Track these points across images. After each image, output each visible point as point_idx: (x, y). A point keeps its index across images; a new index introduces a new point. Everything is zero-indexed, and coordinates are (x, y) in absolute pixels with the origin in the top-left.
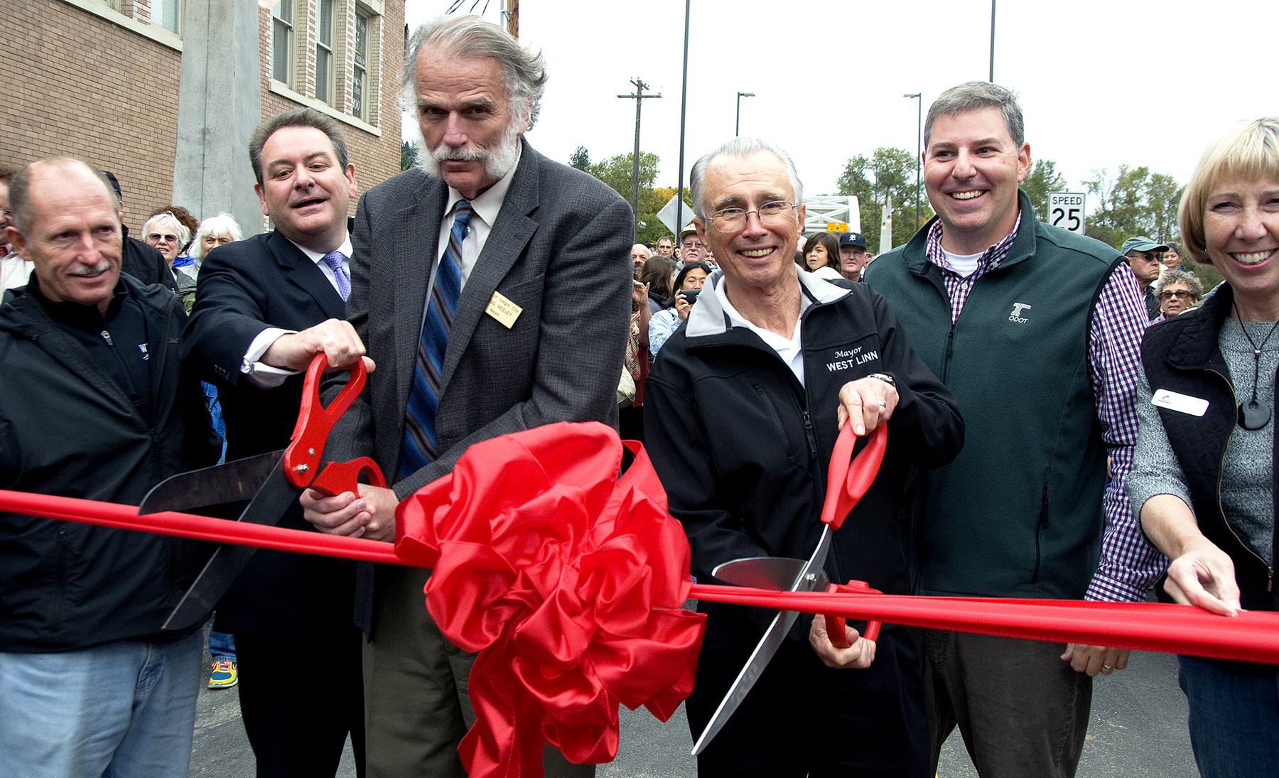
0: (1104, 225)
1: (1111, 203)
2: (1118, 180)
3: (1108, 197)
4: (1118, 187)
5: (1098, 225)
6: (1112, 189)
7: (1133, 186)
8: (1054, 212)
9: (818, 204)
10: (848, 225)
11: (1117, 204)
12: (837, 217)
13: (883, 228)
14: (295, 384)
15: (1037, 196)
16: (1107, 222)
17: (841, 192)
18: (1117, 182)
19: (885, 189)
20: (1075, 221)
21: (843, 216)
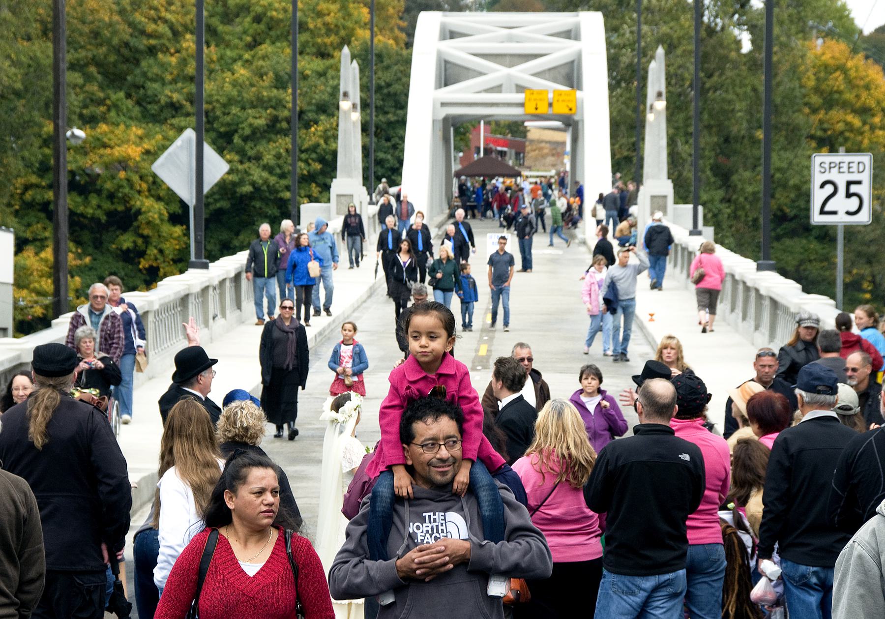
8: (822, 186)
10: (579, 94)
13: (650, 117)
14: (770, 387)
20: (855, 201)
21: (564, 71)
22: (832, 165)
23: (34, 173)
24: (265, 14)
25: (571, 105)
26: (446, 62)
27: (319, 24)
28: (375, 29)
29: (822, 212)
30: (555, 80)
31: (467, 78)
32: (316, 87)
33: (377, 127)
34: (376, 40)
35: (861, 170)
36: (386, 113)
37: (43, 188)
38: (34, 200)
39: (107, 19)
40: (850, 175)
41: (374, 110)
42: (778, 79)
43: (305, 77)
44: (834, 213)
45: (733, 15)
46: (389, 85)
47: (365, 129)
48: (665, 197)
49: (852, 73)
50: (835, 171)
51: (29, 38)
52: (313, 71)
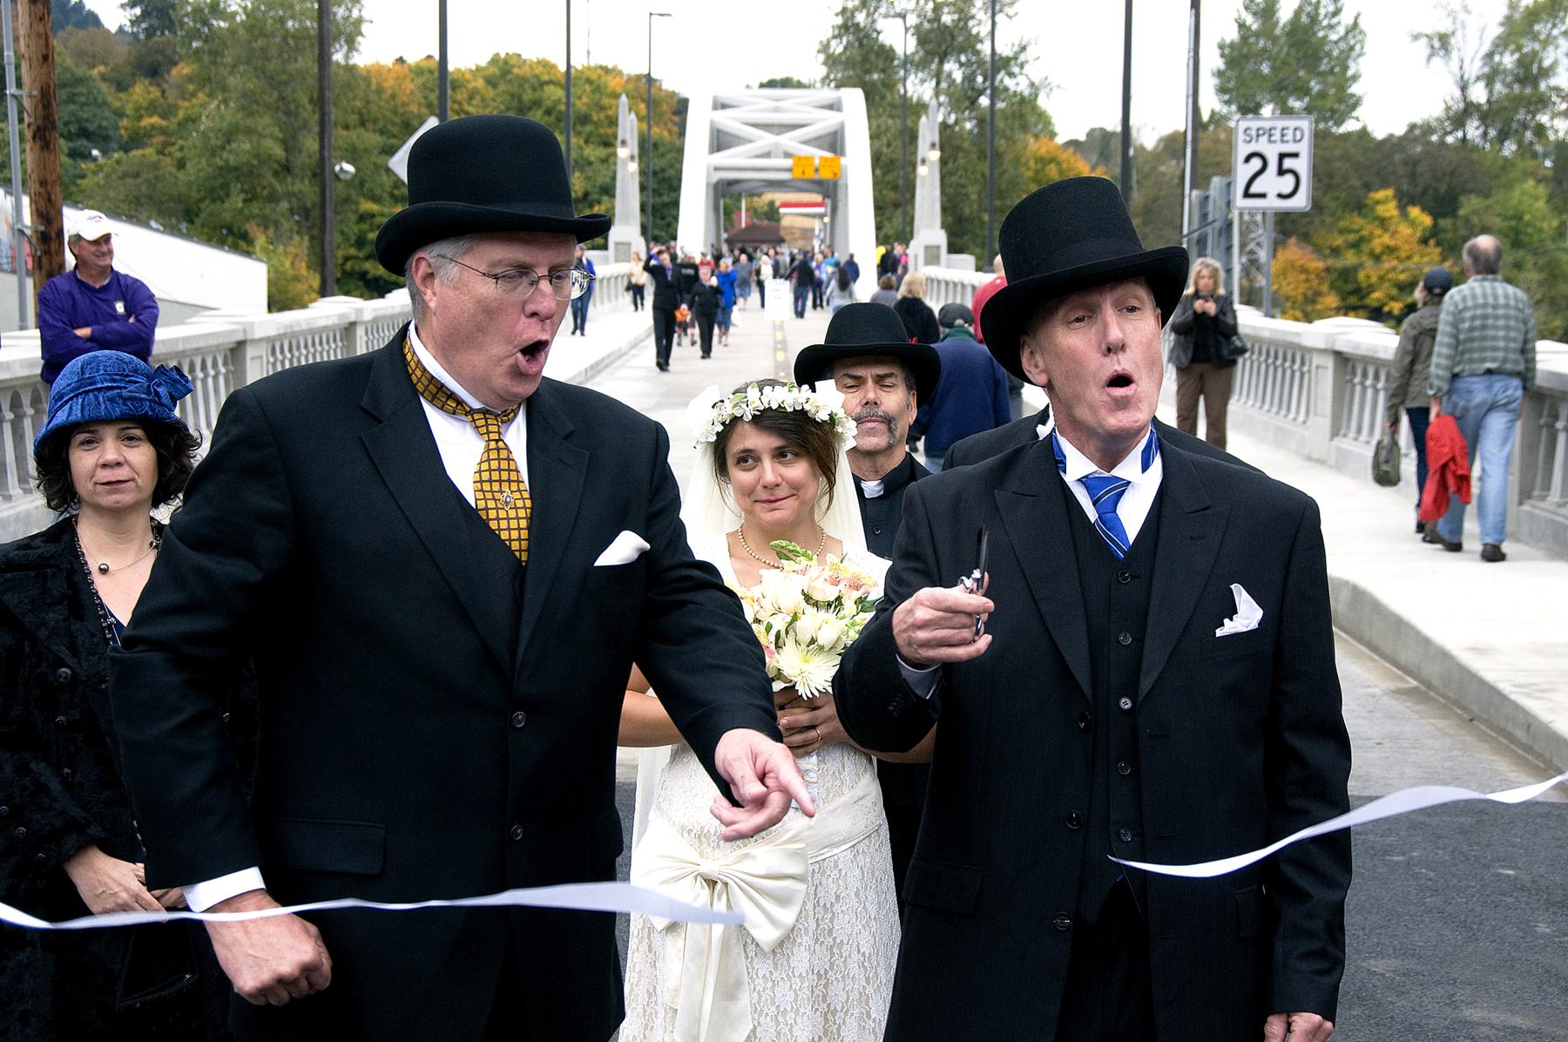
0: (1464, 139)
1: (1481, 85)
2: (1502, 24)
3: (1475, 68)
4: (1501, 44)
5: (1450, 139)
6: (1486, 48)
7: (1535, 37)
8: (1247, 160)
9: (765, 110)
11: (1498, 87)
12: (815, 141)
13: (922, 171)
15: (1302, 73)
16: (1473, 130)
17: (827, 77)
18: (1499, 31)
19: (934, 66)
20: (1289, 179)
22: (1261, 132)
23: (352, 246)
24: (554, 108)
25: (835, 170)
26: (719, 131)
27: (602, 116)
28: (652, 123)
29: (1247, 195)
30: (820, 147)
31: (738, 144)
32: (599, 171)
33: (653, 207)
34: (652, 132)
35: (1298, 137)
36: (660, 195)
37: (360, 259)
38: (353, 270)
39: (416, 111)
40: (1284, 145)
41: (651, 194)
42: (1004, 167)
43: (590, 163)
44: (1263, 196)
45: (964, 111)
46: (663, 170)
47: (643, 209)
48: (938, 247)
49: (1065, 166)
50: (1264, 139)
51: (347, 127)
52: (596, 158)
